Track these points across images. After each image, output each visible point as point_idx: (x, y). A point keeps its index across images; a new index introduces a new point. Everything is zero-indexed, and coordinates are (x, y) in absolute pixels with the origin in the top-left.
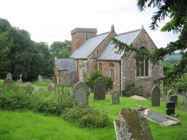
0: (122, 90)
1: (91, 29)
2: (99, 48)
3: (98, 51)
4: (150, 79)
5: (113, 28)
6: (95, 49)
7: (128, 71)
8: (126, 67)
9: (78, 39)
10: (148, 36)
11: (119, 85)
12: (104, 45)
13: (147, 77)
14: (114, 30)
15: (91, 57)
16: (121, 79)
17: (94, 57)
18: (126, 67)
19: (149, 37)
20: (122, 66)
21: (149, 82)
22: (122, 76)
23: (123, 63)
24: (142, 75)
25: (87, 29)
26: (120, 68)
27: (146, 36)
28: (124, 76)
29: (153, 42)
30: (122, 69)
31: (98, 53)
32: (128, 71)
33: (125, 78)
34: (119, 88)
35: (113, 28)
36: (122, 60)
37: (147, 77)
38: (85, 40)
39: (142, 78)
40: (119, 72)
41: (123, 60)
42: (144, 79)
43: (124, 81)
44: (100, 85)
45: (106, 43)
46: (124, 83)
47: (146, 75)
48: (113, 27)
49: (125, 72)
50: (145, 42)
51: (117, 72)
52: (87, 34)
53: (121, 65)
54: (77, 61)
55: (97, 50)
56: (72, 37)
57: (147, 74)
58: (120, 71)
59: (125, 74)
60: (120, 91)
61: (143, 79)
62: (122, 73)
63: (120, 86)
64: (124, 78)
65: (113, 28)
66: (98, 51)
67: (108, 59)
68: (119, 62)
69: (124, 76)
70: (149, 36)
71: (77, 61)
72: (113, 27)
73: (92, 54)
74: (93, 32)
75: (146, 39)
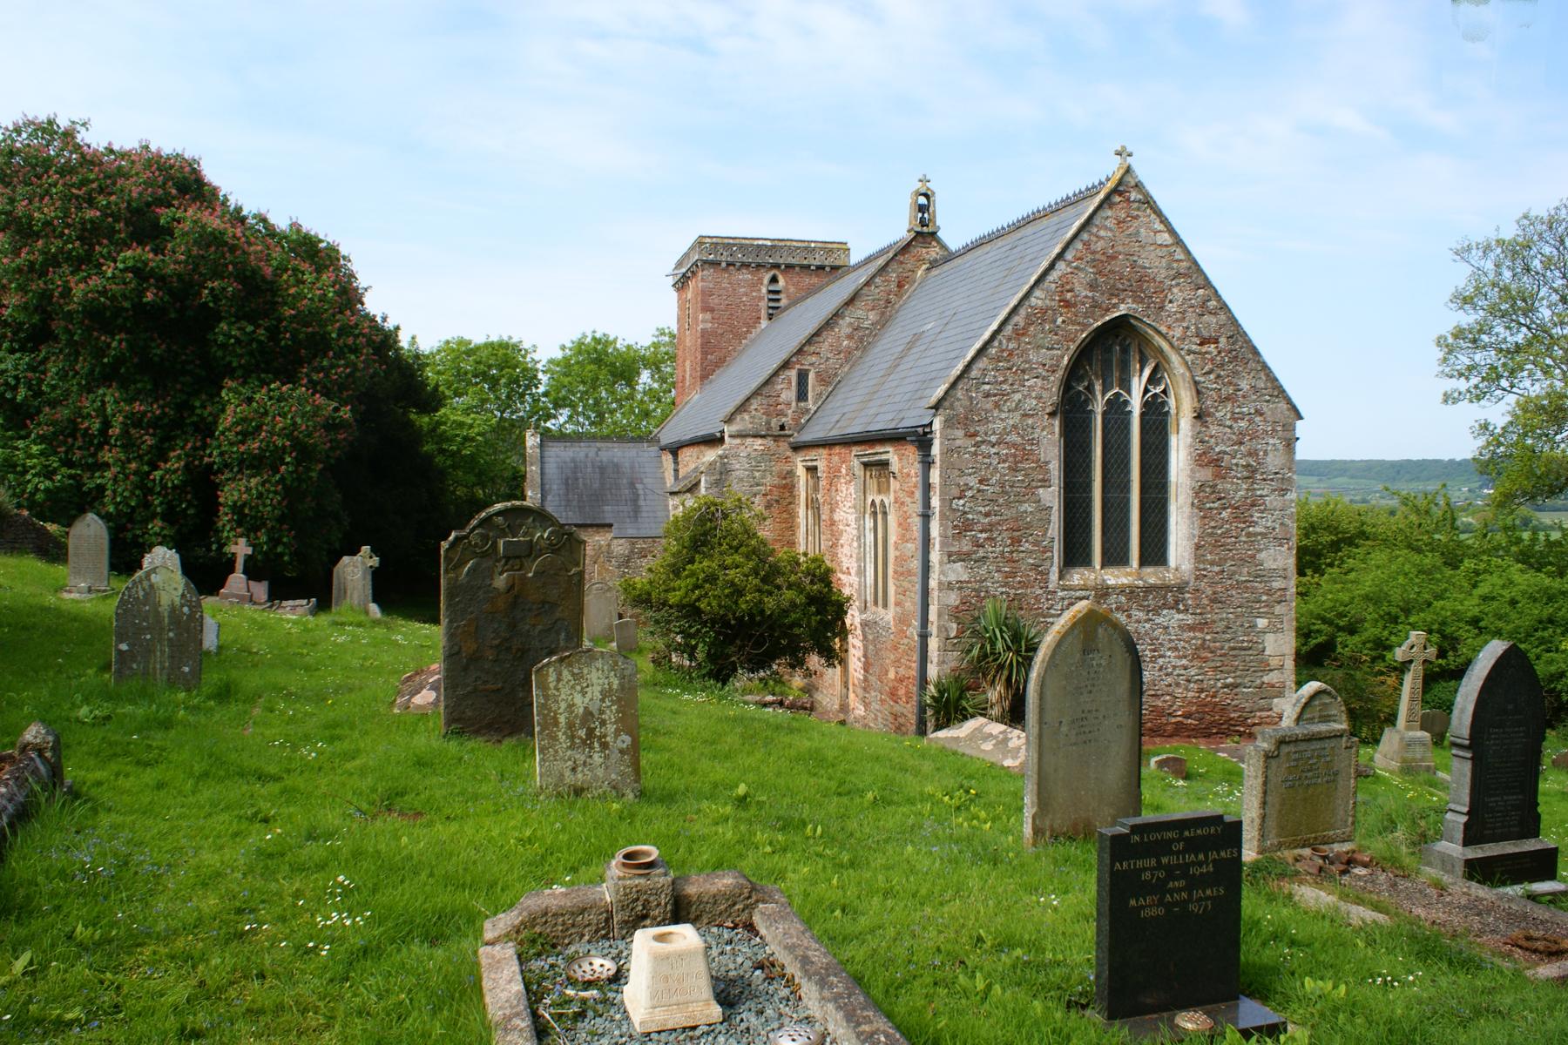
0: (933, 672)
1: (807, 248)
2: (814, 359)
3: (802, 377)
4: (1181, 588)
5: (924, 207)
6: (786, 365)
7: (987, 515)
8: (973, 481)
9: (708, 316)
10: (1166, 238)
11: (914, 631)
12: (850, 337)
13: (1152, 576)
14: (933, 220)
15: (744, 422)
16: (933, 583)
17: (775, 423)
18: (973, 481)
19: (1179, 242)
20: (935, 476)
21: (1172, 618)
22: (935, 556)
23: (947, 452)
24: (1115, 556)
25: (776, 246)
26: (927, 487)
27: (1147, 228)
28: (951, 557)
29: (1207, 284)
30: (935, 502)
31: (802, 395)
32: (987, 515)
33: (959, 572)
34: (916, 657)
35: (924, 207)
36: (937, 425)
37: (1152, 576)
38: (764, 323)
39: (1115, 577)
40: (916, 522)
41: (948, 424)
42: (1131, 592)
43: (953, 599)
44: (501, 581)
45: (873, 316)
46: (955, 614)
47: (1144, 562)
48: (923, 200)
49: (964, 527)
50: (1139, 285)
51: (904, 525)
52: (774, 280)
53: (927, 464)
54: (676, 462)
55: (793, 374)
56: (682, 306)
57: (1154, 552)
58: (926, 517)
59: (966, 546)
60: (923, 681)
61: (1122, 590)
62: (935, 529)
63: (924, 637)
64: (952, 578)
65: (922, 209)
66: (802, 377)
67: (856, 427)
68: (921, 440)
69: (951, 557)
70: (1172, 231)
71: (676, 462)
72: (923, 200)
73: (755, 404)
74: (821, 268)
75: (1154, 263)
